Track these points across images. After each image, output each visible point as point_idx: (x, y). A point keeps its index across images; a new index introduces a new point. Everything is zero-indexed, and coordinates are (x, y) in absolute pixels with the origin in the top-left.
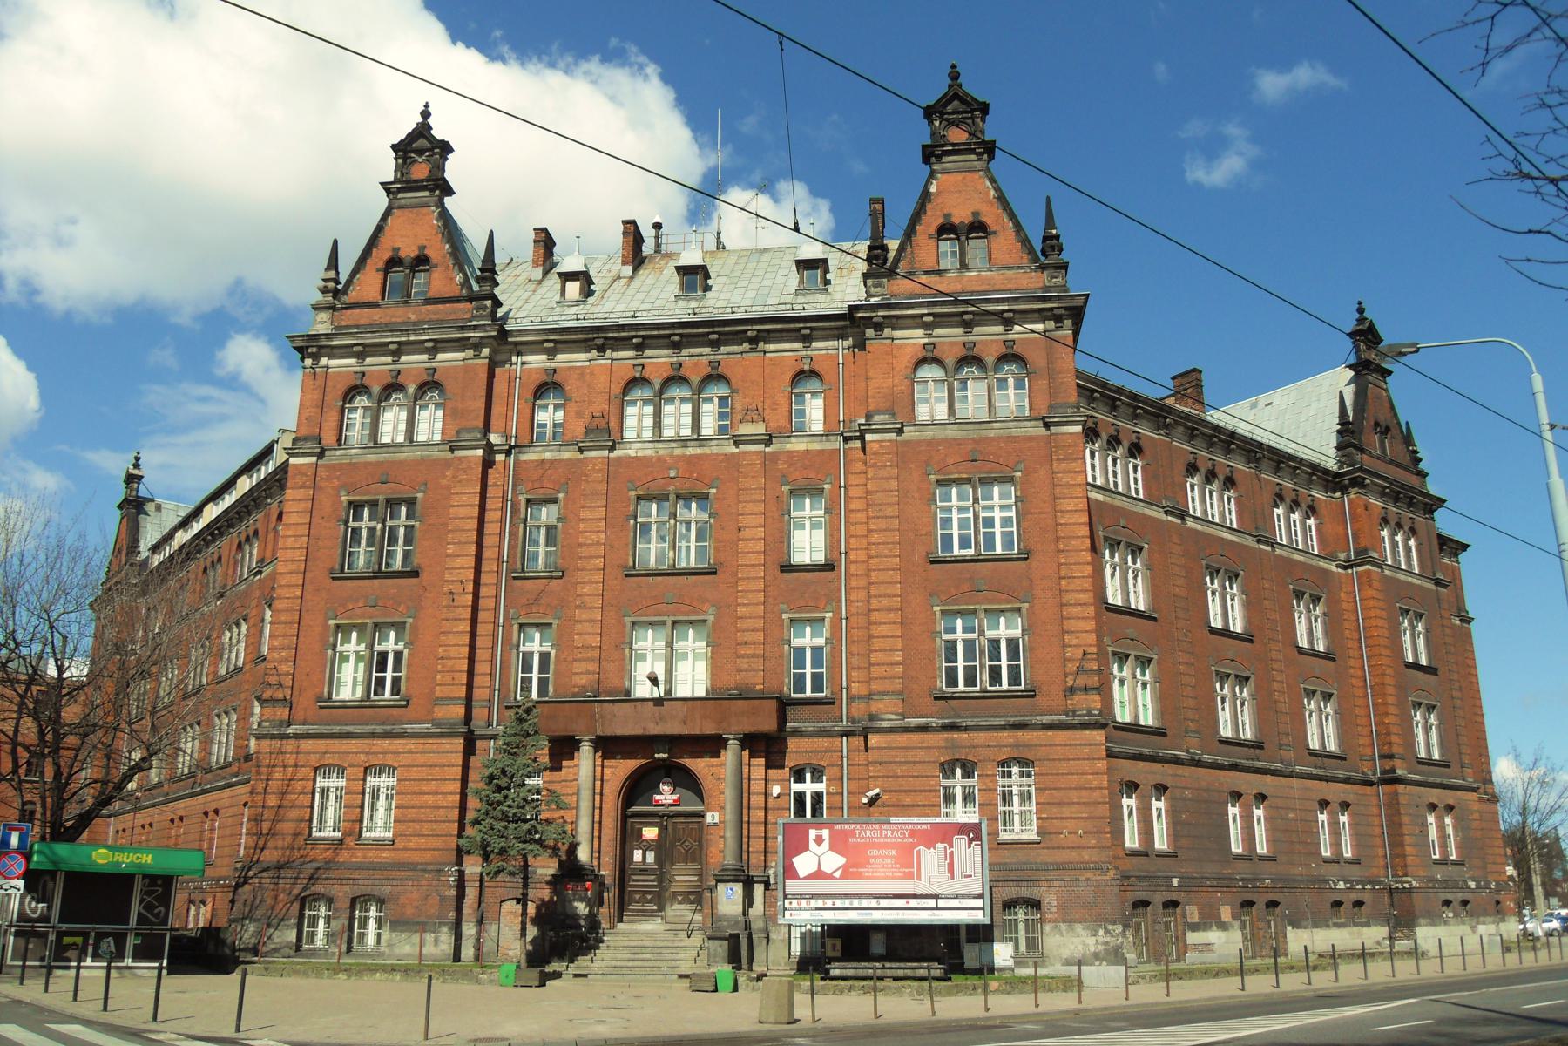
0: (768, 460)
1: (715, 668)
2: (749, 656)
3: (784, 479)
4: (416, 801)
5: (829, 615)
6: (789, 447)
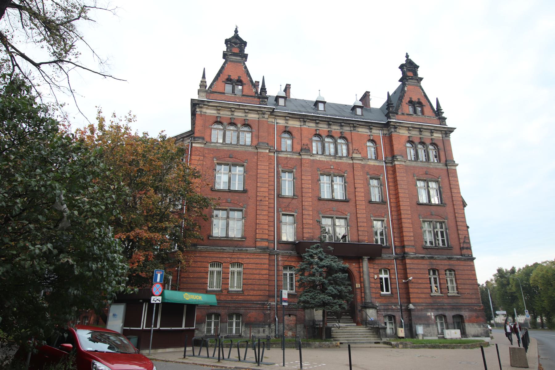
0: (363, 166)
1: (296, 233)
2: (363, 231)
3: (367, 174)
4: (252, 277)
5: (386, 219)
6: (368, 163)
